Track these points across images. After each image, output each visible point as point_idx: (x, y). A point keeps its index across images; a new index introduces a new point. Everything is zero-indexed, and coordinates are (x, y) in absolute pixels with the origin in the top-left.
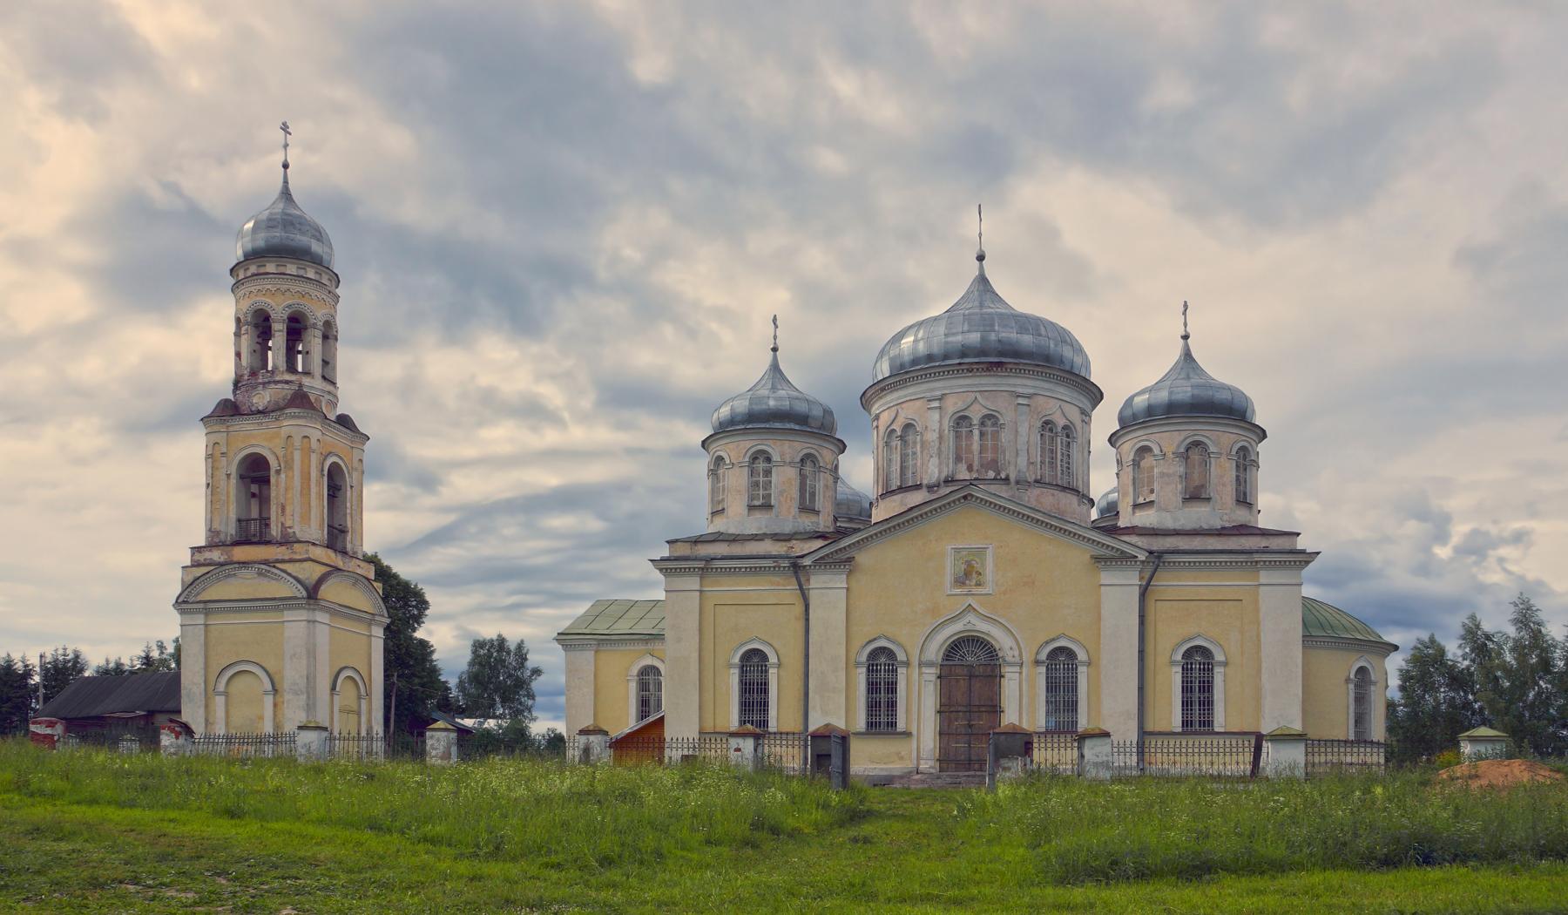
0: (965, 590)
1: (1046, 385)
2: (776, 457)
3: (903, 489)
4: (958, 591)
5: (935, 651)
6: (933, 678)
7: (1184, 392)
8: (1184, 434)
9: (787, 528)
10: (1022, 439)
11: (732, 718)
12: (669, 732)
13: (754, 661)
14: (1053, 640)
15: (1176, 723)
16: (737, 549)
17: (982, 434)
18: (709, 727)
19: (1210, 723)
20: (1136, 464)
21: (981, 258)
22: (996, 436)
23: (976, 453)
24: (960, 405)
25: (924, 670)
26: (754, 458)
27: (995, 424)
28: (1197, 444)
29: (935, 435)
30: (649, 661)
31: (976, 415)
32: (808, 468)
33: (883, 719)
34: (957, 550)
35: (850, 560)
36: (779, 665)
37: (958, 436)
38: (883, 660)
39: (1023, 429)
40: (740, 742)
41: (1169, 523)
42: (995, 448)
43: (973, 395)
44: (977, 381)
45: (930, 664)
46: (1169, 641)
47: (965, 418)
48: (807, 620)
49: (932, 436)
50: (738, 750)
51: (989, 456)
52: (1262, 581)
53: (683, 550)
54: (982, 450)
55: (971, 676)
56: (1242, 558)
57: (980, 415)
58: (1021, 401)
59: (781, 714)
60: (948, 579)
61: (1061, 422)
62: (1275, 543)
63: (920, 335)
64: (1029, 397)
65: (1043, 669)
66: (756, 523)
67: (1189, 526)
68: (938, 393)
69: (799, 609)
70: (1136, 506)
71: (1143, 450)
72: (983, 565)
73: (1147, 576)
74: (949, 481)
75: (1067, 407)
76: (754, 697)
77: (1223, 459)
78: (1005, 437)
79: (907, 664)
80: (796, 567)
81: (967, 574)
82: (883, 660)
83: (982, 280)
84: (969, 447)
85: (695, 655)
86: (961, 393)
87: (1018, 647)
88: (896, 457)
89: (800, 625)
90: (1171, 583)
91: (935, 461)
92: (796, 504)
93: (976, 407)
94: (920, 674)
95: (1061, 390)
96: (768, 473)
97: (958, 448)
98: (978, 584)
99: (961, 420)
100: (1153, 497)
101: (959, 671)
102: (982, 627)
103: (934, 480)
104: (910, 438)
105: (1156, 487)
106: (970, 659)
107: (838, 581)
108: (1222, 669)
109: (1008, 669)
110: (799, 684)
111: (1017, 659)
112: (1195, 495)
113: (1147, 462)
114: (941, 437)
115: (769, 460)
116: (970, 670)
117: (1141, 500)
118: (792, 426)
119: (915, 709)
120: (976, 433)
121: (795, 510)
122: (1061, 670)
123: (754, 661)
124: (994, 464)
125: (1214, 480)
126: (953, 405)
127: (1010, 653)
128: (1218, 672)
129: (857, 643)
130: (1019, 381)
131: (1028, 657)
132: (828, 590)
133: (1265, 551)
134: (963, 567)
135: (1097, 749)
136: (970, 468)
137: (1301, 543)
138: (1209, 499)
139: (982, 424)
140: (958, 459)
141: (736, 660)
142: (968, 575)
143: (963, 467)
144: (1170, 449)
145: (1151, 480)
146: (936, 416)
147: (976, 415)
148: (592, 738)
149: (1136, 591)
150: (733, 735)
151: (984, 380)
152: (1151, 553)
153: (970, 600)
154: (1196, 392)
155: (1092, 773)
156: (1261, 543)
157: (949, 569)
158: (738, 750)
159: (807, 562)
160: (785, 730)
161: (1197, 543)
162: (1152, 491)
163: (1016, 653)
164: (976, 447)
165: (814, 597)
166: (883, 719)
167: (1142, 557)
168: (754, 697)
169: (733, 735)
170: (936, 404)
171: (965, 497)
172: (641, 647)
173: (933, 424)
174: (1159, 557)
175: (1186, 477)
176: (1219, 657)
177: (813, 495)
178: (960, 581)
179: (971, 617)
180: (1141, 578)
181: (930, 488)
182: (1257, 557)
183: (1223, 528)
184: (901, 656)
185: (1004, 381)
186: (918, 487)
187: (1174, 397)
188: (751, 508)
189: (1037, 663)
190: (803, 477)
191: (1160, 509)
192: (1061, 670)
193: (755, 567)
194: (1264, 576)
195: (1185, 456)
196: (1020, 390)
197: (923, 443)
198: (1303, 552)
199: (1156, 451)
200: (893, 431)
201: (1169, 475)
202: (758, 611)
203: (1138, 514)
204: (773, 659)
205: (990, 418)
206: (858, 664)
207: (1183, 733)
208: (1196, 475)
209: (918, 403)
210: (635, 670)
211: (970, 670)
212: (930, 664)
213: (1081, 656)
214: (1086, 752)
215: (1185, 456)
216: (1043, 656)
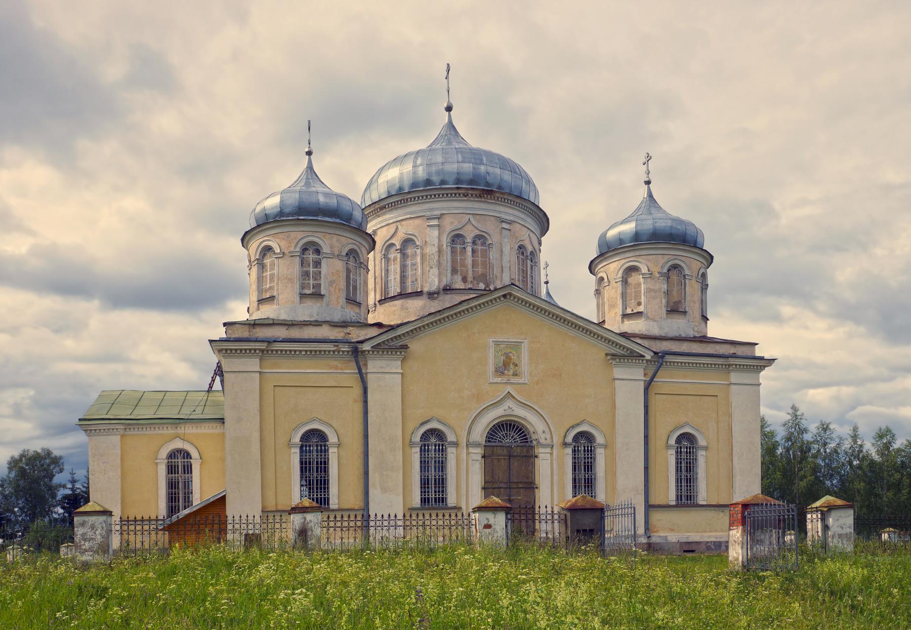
0: (505, 380)
1: (522, 216)
2: (326, 249)
3: (402, 295)
4: (499, 380)
5: (479, 433)
6: (479, 457)
7: (648, 225)
8: (666, 258)
9: (337, 317)
10: (506, 258)
11: (295, 494)
12: (232, 510)
13: (314, 449)
14: (573, 427)
15: (672, 499)
16: (295, 333)
17: (473, 251)
18: (271, 506)
19: (443, 500)
20: (625, 282)
21: (449, 109)
22: (485, 254)
23: (470, 267)
24: (457, 225)
25: (471, 450)
26: (304, 250)
27: (483, 244)
28: (675, 267)
29: (435, 249)
30: (178, 444)
31: (469, 234)
32: (311, 256)
33: (432, 496)
34: (497, 344)
35: (405, 347)
36: (339, 446)
37: (453, 252)
38: (433, 440)
39: (506, 250)
40: (490, 517)
41: (656, 332)
42: (484, 264)
43: (467, 217)
44: (470, 205)
45: (477, 445)
46: (665, 430)
47: (459, 236)
48: (366, 402)
49: (431, 250)
50: (488, 526)
51: (480, 270)
52: (733, 380)
53: (244, 333)
54: (474, 264)
55: (510, 456)
56: (720, 361)
57: (473, 235)
58: (505, 225)
59: (341, 490)
60: (491, 368)
61: (530, 248)
62: (740, 351)
63: (419, 161)
64: (510, 223)
65: (569, 451)
66: (309, 311)
67: (672, 334)
68: (438, 213)
69: (357, 391)
70: (625, 316)
71: (632, 269)
72: (519, 357)
73: (651, 374)
74: (447, 290)
75: (532, 234)
76: (315, 474)
77: (694, 281)
78: (493, 255)
79: (456, 444)
80: (356, 352)
81: (506, 365)
82: (433, 440)
83: (451, 126)
84: (463, 261)
85: (256, 435)
86: (459, 214)
87: (548, 430)
88: (395, 268)
89: (358, 408)
90: (667, 379)
91: (435, 271)
92: (343, 295)
93: (469, 227)
94: (468, 453)
95: (529, 220)
96: (317, 264)
97: (454, 261)
98: (515, 375)
99: (457, 238)
100: (641, 309)
101: (499, 451)
102: (520, 413)
103: (434, 288)
104: (409, 251)
105: (643, 300)
106: (507, 441)
107: (395, 365)
108: (704, 453)
109: (541, 450)
110: (358, 463)
111: (549, 442)
112: (675, 309)
113: (635, 278)
114: (440, 251)
115: (318, 252)
116: (509, 449)
117: (629, 311)
118: (338, 221)
119: (463, 485)
120: (469, 249)
121: (342, 300)
122: (583, 447)
123: (314, 449)
124: (483, 278)
125: (688, 298)
126: (450, 224)
127: (543, 436)
128: (701, 456)
129: (411, 426)
130: (502, 209)
131: (557, 440)
132: (384, 374)
133: (734, 356)
134: (502, 358)
135: (842, 521)
136: (464, 280)
137: (758, 352)
138: (685, 313)
139: (474, 243)
140: (454, 271)
141: (297, 439)
142: (506, 366)
143: (458, 278)
144: (656, 270)
145: (638, 295)
146: (436, 233)
147: (469, 234)
148: (309, 517)
149: (641, 386)
150: (295, 510)
151: (477, 205)
152: (655, 353)
153: (509, 388)
154: (674, 225)
155: (832, 543)
156: (731, 350)
157: (491, 359)
158: (488, 526)
159: (366, 347)
160: (280, 508)
161: (685, 347)
162: (639, 304)
163: (548, 437)
164: (469, 261)
165: (371, 380)
166: (432, 496)
167: (648, 357)
168: (315, 474)
169: (295, 510)
170: (435, 222)
171: (504, 296)
172: (171, 431)
173: (432, 239)
174: (662, 357)
175: (668, 293)
176: (702, 442)
177: (355, 288)
178: (500, 371)
179: (509, 403)
180: (645, 375)
181: (432, 295)
182: (732, 361)
183: (695, 337)
184: (451, 437)
185: (491, 207)
186: (418, 294)
187: (639, 228)
188: (303, 296)
189: (565, 444)
190: (348, 271)
191: (648, 318)
192: (583, 447)
193: (313, 350)
194: (735, 377)
195: (667, 276)
196: (503, 216)
197: (423, 256)
198: (762, 358)
199: (644, 270)
200: (393, 245)
201: (655, 291)
202: (320, 395)
203: (626, 322)
204: (332, 439)
205: (480, 238)
206: (412, 444)
207: (676, 506)
208: (675, 293)
209: (417, 221)
210: (164, 453)
211: (509, 449)
212: (477, 445)
213: (600, 439)
214: (830, 521)
215: (667, 276)
216: (569, 439)
